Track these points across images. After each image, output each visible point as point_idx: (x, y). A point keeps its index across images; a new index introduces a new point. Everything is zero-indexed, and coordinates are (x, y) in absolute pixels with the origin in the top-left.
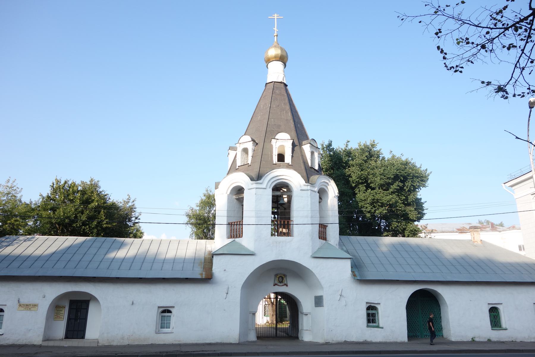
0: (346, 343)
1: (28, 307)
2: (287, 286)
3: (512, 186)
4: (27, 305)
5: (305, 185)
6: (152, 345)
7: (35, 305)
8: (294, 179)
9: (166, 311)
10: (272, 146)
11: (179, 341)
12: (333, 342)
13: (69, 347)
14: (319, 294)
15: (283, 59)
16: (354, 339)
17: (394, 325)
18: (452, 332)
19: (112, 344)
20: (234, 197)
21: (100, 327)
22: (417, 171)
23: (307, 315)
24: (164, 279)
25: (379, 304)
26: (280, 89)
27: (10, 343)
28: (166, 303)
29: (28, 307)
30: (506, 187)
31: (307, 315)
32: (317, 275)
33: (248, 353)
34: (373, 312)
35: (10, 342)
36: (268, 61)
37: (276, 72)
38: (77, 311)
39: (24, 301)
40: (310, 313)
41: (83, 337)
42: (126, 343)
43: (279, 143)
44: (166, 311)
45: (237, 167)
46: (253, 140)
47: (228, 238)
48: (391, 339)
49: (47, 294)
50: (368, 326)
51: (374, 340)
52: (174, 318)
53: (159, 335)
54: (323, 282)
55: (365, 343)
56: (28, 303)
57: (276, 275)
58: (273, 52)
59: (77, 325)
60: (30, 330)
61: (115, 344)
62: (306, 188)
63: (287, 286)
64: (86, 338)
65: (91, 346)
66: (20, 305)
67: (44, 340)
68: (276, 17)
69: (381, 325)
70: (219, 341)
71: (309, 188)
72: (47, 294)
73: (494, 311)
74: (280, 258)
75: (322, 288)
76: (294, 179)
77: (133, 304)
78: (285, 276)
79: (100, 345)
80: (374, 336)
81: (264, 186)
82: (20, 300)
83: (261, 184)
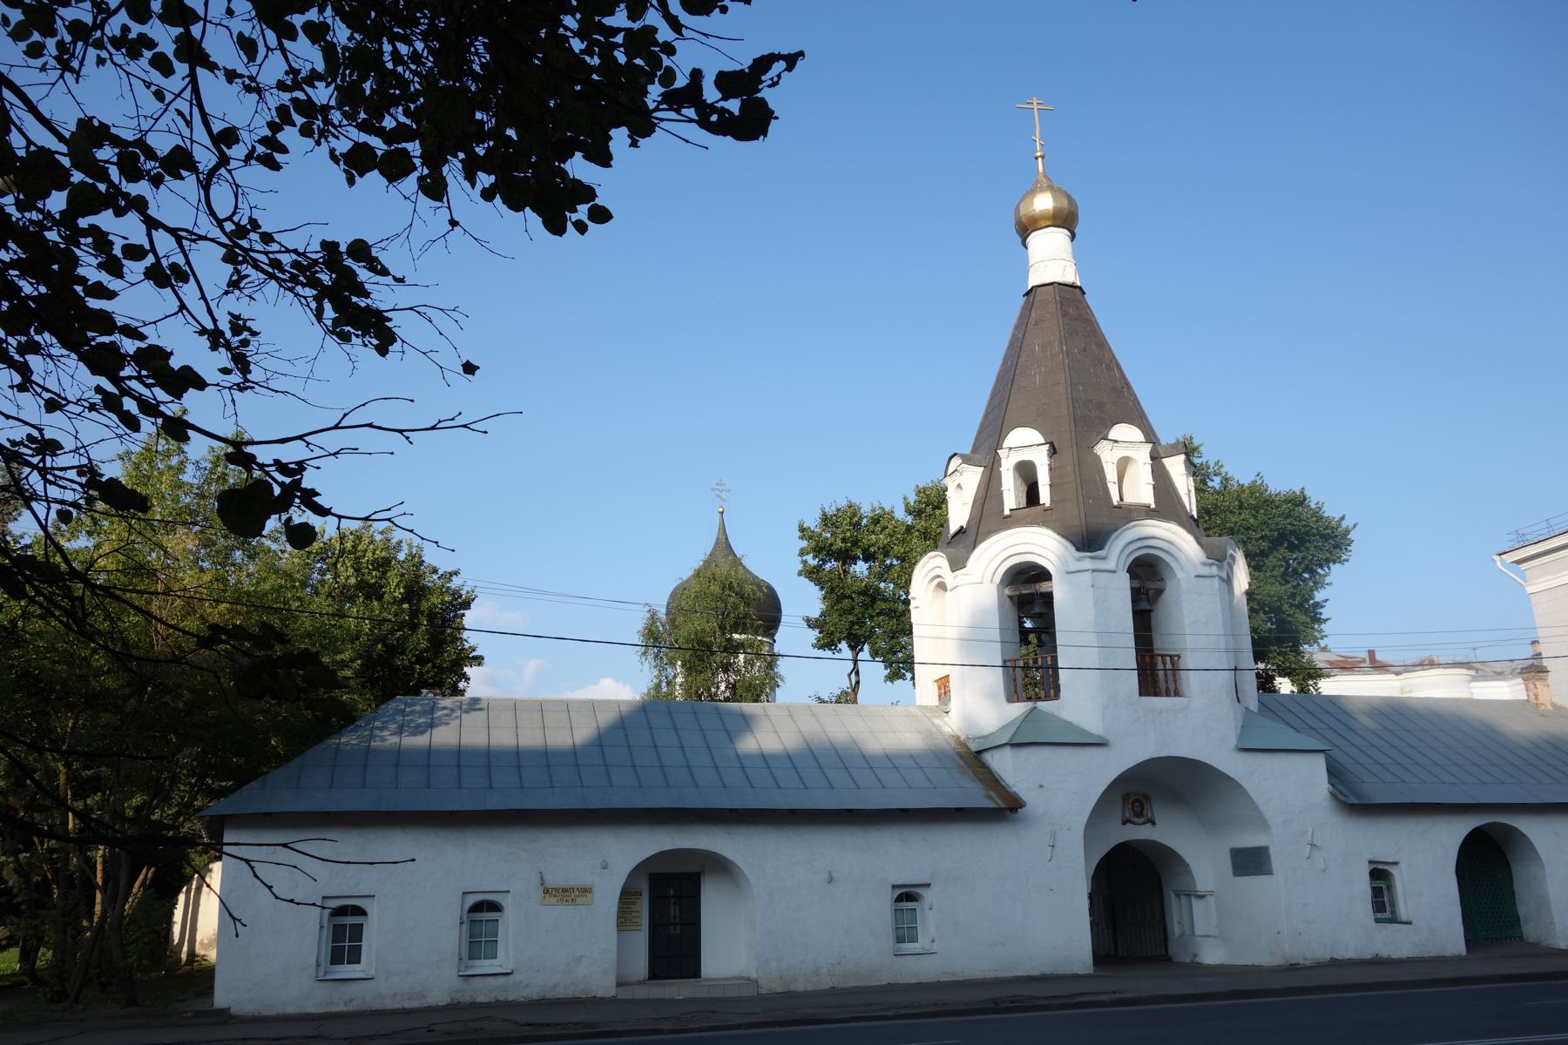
0: (1334, 963)
1: (569, 894)
2: (1154, 824)
3: (1519, 562)
4: (565, 890)
5: (1204, 564)
6: (891, 988)
7: (586, 891)
8: (1179, 543)
9: (907, 896)
10: (1098, 459)
11: (953, 974)
12: (1307, 963)
13: (643, 1001)
14: (1250, 840)
15: (1065, 219)
16: (1350, 953)
17: (1433, 918)
18: (1558, 927)
19: (793, 987)
20: (1007, 591)
21: (740, 944)
22: (1317, 515)
23: (1202, 897)
24: (902, 810)
25: (1396, 863)
26: (1067, 300)
27: (535, 997)
28: (908, 876)
29: (569, 894)
30: (1503, 562)
31: (1202, 897)
32: (1254, 796)
33: (1288, 989)
34: (910, 905)
35: (534, 993)
36: (1025, 228)
37: (1050, 258)
38: (670, 905)
39: (556, 879)
40: (1212, 893)
41: (695, 972)
42: (826, 983)
43: (1119, 453)
44: (907, 896)
45: (1007, 512)
46: (1052, 444)
47: (1010, 700)
48: (1432, 951)
49: (616, 857)
50: (1377, 921)
51: (1395, 956)
52: (930, 918)
53: (902, 959)
54: (1268, 812)
55: (1377, 962)
56: (567, 885)
57: (1126, 797)
58: (1044, 203)
59: (675, 946)
60: (580, 959)
61: (799, 986)
62: (1206, 571)
63: (1154, 824)
64: (703, 974)
65: (743, 994)
66: (547, 891)
67: (619, 985)
68: (1036, 107)
69: (1403, 916)
70: (1047, 970)
71: (1214, 570)
72: (616, 857)
73: (483, 911)
74: (1165, 753)
75: (1262, 824)
76: (1179, 543)
77: (831, 880)
78: (1148, 798)
79: (764, 991)
80: (1396, 943)
81: (1111, 564)
82: (546, 877)
83: (1104, 558)
